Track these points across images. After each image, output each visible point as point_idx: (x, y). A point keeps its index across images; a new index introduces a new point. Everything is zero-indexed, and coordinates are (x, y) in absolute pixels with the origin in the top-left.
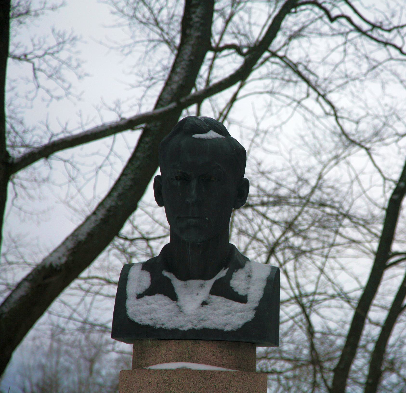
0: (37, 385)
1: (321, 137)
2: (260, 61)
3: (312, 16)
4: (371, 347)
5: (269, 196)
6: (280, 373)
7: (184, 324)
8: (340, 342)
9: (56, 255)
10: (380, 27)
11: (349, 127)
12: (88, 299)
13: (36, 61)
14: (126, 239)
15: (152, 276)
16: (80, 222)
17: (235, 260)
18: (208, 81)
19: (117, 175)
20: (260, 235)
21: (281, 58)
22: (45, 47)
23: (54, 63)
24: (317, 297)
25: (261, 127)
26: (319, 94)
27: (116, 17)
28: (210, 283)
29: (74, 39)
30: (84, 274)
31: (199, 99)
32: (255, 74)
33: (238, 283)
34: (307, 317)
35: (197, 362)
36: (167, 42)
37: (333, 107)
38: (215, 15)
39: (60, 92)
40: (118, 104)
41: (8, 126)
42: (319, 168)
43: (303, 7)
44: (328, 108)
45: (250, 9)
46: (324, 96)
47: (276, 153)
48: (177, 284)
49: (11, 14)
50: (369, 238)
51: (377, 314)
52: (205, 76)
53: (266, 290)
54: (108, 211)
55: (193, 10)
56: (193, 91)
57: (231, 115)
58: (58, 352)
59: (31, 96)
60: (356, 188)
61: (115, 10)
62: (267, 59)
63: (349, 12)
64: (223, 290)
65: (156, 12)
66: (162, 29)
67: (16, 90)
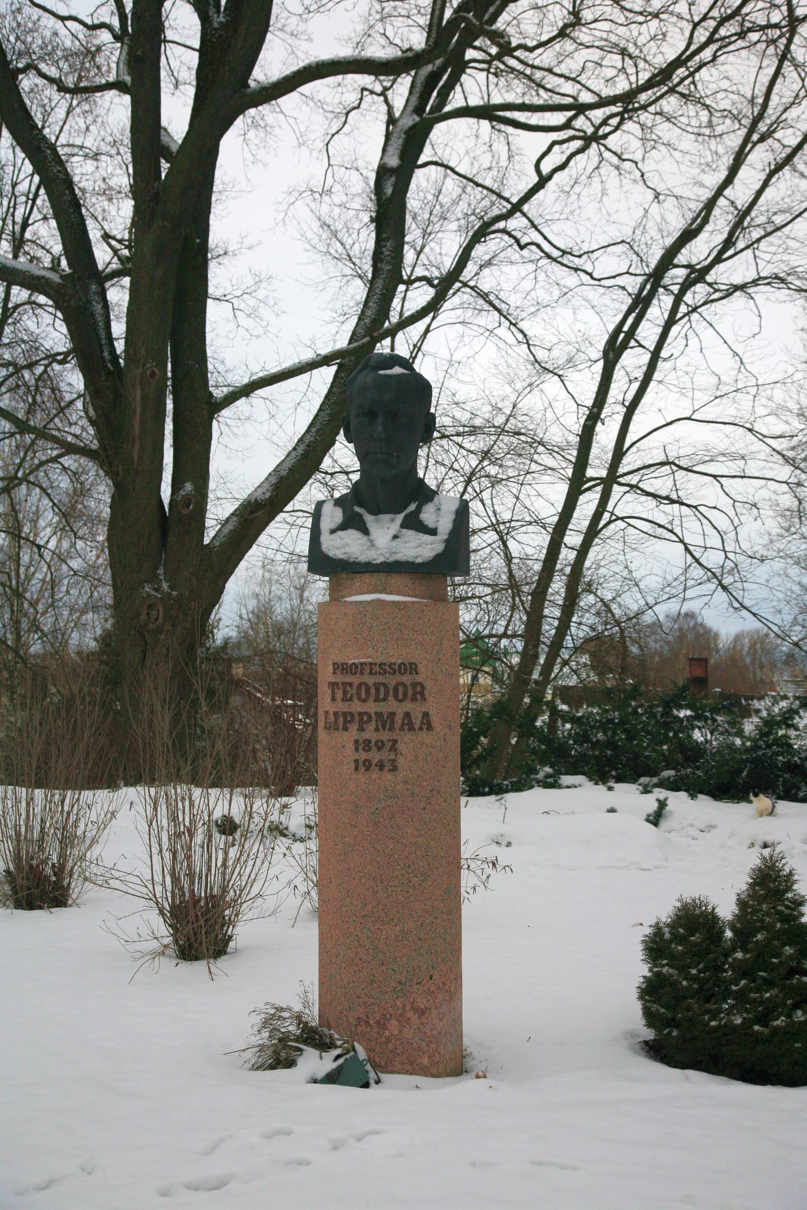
0: (253, 612)
1: (514, 366)
2: (451, 291)
3: (503, 244)
4: (568, 570)
5: (464, 426)
6: (480, 598)
7: (377, 556)
8: (538, 567)
9: (260, 491)
10: (570, 253)
11: (541, 354)
12: (294, 531)
13: (234, 301)
14: (326, 473)
15: (344, 512)
16: (283, 458)
17: (425, 494)
18: (401, 314)
19: (315, 411)
20: (456, 466)
21: (472, 288)
22: (243, 287)
23: (252, 302)
24: (513, 524)
25: (454, 358)
26: (511, 323)
27: (310, 254)
28: (400, 518)
29: (270, 277)
30: (288, 508)
31: (392, 333)
32: (447, 305)
33: (428, 516)
34: (505, 544)
35: (391, 593)
36: (360, 277)
37: (525, 336)
38: (406, 247)
39: (259, 331)
40: (313, 340)
41: (210, 367)
42: (513, 398)
43: (492, 236)
44: (520, 337)
45: (441, 239)
46: (515, 325)
47: (470, 383)
48: (369, 518)
49: (209, 255)
50: (564, 465)
51: (573, 539)
52: (399, 309)
53: (455, 522)
54: (308, 446)
55: (383, 243)
56: (387, 324)
57: (424, 347)
58: (270, 581)
59: (231, 336)
60: (550, 415)
61: (308, 247)
62: (458, 290)
63: (539, 239)
64: (414, 523)
65: (348, 247)
66: (354, 264)
67: (216, 331)
